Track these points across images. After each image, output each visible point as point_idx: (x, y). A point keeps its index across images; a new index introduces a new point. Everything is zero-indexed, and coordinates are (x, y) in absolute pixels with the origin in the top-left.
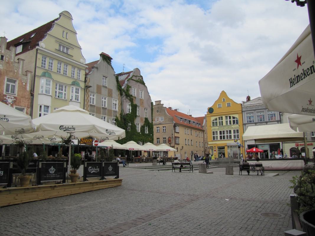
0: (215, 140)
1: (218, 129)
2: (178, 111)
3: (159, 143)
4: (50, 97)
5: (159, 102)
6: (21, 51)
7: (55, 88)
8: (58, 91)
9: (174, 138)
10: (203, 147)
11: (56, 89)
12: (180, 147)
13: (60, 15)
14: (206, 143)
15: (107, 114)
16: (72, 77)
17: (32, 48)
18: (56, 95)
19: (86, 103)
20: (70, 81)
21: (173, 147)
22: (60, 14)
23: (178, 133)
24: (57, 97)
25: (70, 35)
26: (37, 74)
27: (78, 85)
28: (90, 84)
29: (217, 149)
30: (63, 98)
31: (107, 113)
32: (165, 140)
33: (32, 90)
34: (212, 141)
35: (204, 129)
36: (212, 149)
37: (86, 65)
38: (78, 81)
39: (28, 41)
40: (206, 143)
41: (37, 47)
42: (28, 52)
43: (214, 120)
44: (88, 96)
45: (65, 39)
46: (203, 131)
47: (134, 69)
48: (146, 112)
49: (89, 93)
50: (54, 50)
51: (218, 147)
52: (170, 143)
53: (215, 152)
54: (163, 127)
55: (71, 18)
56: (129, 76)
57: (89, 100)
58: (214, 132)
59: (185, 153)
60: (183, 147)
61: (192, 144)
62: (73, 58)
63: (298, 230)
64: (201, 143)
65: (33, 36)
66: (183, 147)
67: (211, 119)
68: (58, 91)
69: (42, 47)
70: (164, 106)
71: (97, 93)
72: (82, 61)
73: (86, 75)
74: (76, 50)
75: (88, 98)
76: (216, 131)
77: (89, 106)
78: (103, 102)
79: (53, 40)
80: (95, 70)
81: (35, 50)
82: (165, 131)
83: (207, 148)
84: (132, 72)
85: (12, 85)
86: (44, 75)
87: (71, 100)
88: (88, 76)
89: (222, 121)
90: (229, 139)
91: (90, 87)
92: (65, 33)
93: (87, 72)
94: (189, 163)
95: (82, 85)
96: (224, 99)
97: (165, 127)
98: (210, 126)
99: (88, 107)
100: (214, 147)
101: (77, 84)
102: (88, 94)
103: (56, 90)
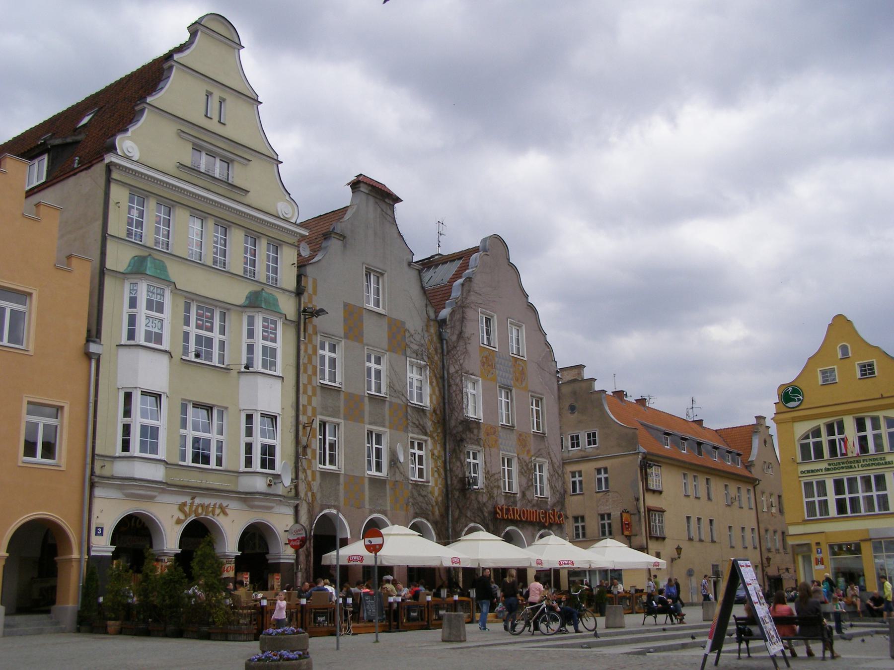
0: (818, 517)
1: (828, 470)
2: (651, 406)
3: (584, 535)
4: (165, 359)
5: (575, 371)
6: (44, 180)
7: (182, 322)
8: (193, 331)
10: (755, 548)
11: (187, 322)
12: (668, 548)
13: (194, 30)
14: (767, 531)
15: (387, 423)
16: (249, 276)
17: (87, 164)
18: (186, 350)
19: (303, 379)
20: (238, 294)
21: (643, 549)
22: (194, 27)
23: (656, 495)
24: (191, 357)
25: (234, 108)
26: (109, 265)
27: (272, 308)
28: (318, 304)
29: (826, 554)
30: (215, 361)
31: (387, 417)
33: (94, 332)
34: (805, 522)
35: (756, 473)
36: (804, 557)
37: (303, 225)
38: (268, 290)
39: (69, 140)
40: (767, 531)
41: (109, 158)
42: (71, 181)
43: (807, 437)
44: (310, 351)
45: (214, 126)
46: (753, 482)
47: (484, 241)
48: (537, 411)
49: (314, 337)
50: (170, 167)
51: (831, 547)
52: (627, 533)
53: (821, 567)
54: (599, 471)
55: (237, 41)
56: (465, 267)
57: (315, 368)
58: (808, 485)
59: (690, 573)
60: (679, 549)
61: (715, 539)
62: (250, 199)
64: (748, 534)
65: (86, 120)
66: (679, 549)
67: (793, 428)
68: (193, 331)
69: (128, 158)
70: (598, 387)
71: (346, 337)
72: (283, 208)
73: (302, 265)
74: (257, 167)
75: (314, 357)
76: (820, 478)
77: (318, 390)
78: (369, 375)
79: (169, 129)
80: (334, 244)
81: (99, 170)
82: (607, 487)
83: (773, 550)
84: (476, 250)
85: (12, 310)
86: (138, 269)
87: (247, 367)
88: (309, 270)
89: (606, 476)
90: (877, 511)
91: (320, 312)
92: (214, 103)
93: (306, 253)
95: (288, 306)
96: (844, 349)
97: (580, 473)
98: (794, 460)
99: (314, 394)
100: (814, 548)
101: (267, 302)
102: (310, 341)
103: (186, 328)
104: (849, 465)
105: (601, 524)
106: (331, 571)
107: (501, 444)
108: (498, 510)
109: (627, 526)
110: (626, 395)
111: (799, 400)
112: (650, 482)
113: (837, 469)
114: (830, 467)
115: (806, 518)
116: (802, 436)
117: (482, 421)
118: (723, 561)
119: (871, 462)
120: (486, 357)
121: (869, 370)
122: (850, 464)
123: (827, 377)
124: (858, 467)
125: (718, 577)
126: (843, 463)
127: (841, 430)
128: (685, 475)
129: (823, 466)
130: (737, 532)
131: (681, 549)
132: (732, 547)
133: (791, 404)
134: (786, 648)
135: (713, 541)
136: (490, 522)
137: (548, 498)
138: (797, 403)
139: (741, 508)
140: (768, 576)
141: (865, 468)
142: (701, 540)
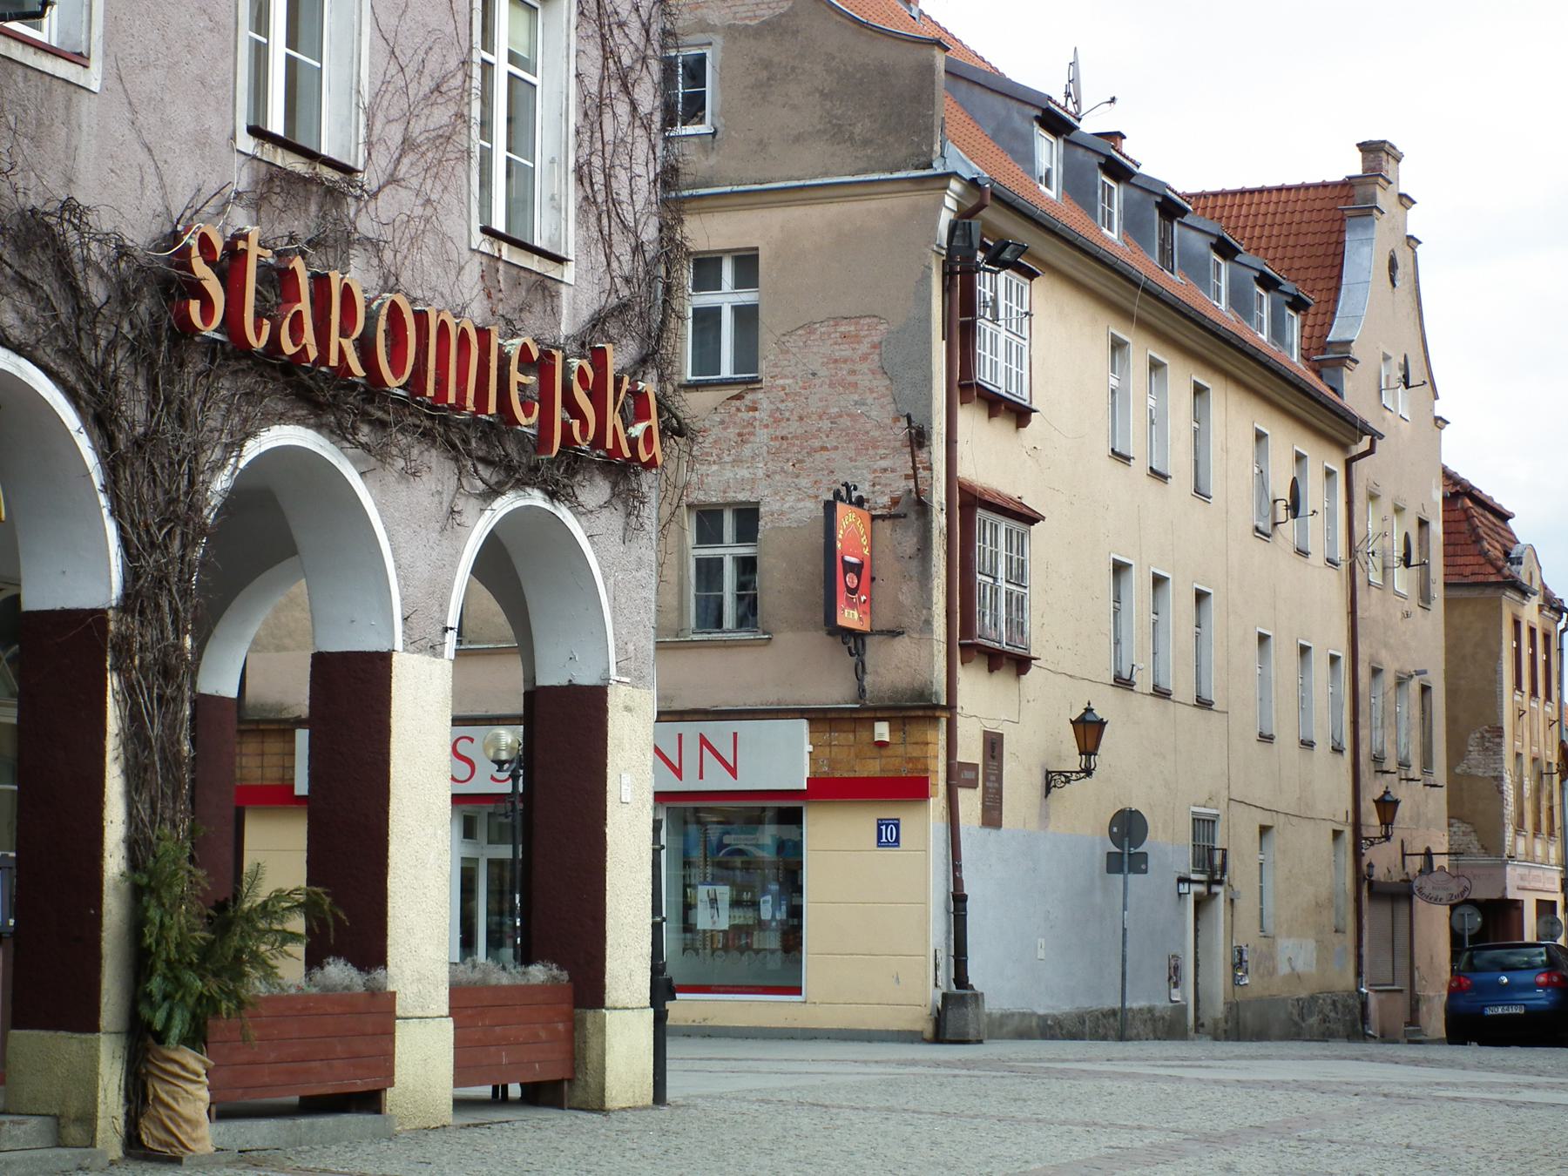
9: (939, 520)
10: (1338, 750)
14: (1376, 672)
32: (729, 552)
35: (1356, 394)
60: (1089, 730)
66: (1089, 730)
89: (747, 297)
97: (747, 266)
105: (699, 561)
106: (565, 976)
108: (201, 269)
109: (851, 580)
112: (983, 351)
125: (1211, 882)
128: (1117, 345)
131: (1101, 724)
132: (1267, 738)
135: (1203, 704)
136: (121, 361)
137: (560, 260)
139: (1302, 553)
140: (1371, 884)
142: (1161, 693)
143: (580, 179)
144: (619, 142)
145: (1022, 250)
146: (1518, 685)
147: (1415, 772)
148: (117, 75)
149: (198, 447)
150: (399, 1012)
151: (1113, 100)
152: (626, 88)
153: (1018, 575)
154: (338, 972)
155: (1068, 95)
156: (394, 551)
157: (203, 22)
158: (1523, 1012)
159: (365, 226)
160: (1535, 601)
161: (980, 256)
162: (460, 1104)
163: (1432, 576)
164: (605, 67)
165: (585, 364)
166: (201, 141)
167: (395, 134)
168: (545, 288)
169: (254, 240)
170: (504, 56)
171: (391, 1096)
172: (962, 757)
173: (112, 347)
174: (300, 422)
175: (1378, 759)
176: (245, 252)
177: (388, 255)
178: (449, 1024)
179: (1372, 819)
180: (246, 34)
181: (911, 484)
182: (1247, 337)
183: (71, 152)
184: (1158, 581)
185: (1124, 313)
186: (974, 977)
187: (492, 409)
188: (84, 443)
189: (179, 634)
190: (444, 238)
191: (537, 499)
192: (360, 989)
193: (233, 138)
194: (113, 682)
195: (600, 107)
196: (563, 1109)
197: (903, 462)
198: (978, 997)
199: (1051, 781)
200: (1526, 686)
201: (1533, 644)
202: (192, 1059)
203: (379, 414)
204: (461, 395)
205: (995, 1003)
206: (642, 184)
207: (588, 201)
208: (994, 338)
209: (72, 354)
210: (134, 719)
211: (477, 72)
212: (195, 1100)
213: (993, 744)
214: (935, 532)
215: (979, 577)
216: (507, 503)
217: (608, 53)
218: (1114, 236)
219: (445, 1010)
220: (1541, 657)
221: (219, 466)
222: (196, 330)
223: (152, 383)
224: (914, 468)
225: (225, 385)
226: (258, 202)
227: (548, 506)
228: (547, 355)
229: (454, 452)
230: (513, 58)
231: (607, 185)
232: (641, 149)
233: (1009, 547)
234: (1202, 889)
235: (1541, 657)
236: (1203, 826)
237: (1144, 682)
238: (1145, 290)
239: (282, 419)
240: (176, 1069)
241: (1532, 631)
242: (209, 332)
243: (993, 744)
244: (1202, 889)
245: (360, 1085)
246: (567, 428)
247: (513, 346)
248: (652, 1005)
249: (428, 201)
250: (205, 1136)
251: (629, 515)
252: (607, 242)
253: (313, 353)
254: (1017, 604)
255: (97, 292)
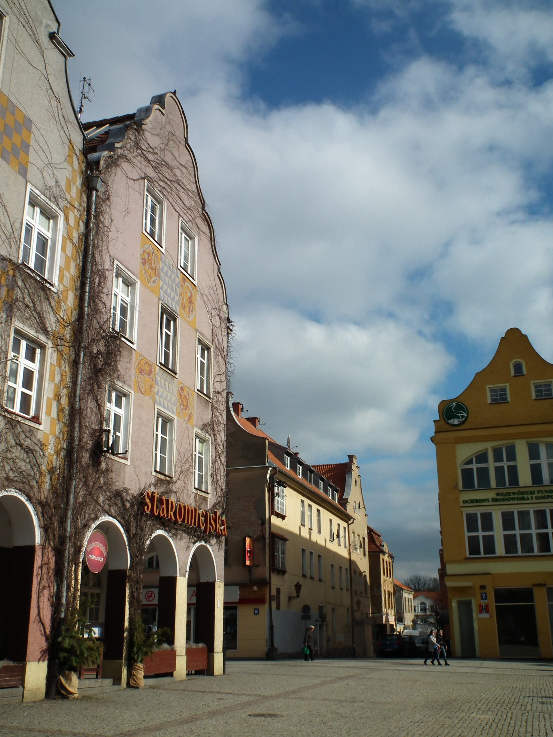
9: (267, 541)
10: (347, 590)
53: (485, 615)
60: (298, 587)
63: (186, 646)
66: (298, 587)
89: (511, 463)
94: (70, 589)
96: (518, 368)
104: (521, 496)
106: (206, 646)
107: (157, 393)
108: (148, 500)
110: (242, 409)
111: (463, 417)
113: (507, 500)
114: (498, 497)
115: (468, 555)
116: (464, 461)
117: (134, 347)
118: (326, 602)
119: (547, 494)
120: (149, 254)
121: (546, 390)
122: (522, 496)
123: (501, 395)
124: (532, 499)
126: (514, 493)
127: (512, 456)
128: (302, 501)
129: (490, 495)
130: (336, 569)
133: (453, 421)
134: (152, 644)
135: (320, 580)
138: (460, 420)
141: (539, 501)
142: (312, 578)
143: (211, 477)
144: (218, 469)
145: (284, 482)
146: (384, 574)
147: (364, 595)
148: (132, 462)
149: (144, 536)
150: (177, 655)
151: (297, 446)
152: (220, 458)
153: (283, 553)
154: (166, 646)
155: (287, 445)
156: (178, 555)
157: (147, 450)
158: (417, 645)
159: (174, 489)
160: (387, 555)
161: (275, 484)
162: (188, 674)
163: (366, 550)
164: (216, 454)
165: (213, 515)
166: (146, 474)
167: (179, 470)
168: (205, 499)
169: (156, 494)
170: (198, 452)
171: (174, 672)
172: (272, 594)
173: (130, 516)
174: (162, 529)
175: (356, 592)
176: (155, 496)
177: (178, 494)
178: (185, 657)
179: (355, 606)
180: (154, 452)
181: (261, 533)
182: (327, 498)
183: (124, 477)
184: (311, 553)
185: (303, 495)
186: (275, 645)
187: (197, 525)
188: (124, 535)
189: (140, 574)
190: (188, 490)
191: (203, 543)
192: (170, 649)
193: (152, 473)
194: (127, 585)
195: (215, 462)
196: (205, 675)
197: (260, 528)
198: (276, 649)
199: (290, 599)
200: (386, 574)
201: (384, 563)
202: (141, 665)
203: (176, 527)
204: (191, 523)
205: (280, 650)
206: (223, 477)
207: (213, 481)
208: (278, 501)
209: (123, 518)
210: (131, 592)
211: (194, 456)
212: (140, 674)
213: (278, 591)
214: (267, 543)
215: (276, 553)
216: (198, 544)
217: (217, 451)
218: (288, 469)
219: (185, 654)
220: (388, 568)
221: (147, 539)
222: (145, 512)
223: (137, 523)
224: (262, 529)
225: (149, 523)
226: (155, 485)
227: (205, 544)
228: (206, 513)
229: (189, 534)
230: (199, 453)
231: (216, 478)
232: (222, 469)
233: (281, 547)
234: (321, 623)
235: (388, 568)
236: (321, 608)
237: (308, 576)
238: (308, 490)
239: (158, 529)
240: (137, 667)
241: (387, 562)
242: (148, 512)
243: (278, 591)
244: (321, 623)
245: (169, 671)
246: (210, 528)
247: (200, 512)
248: (223, 652)
249: (185, 483)
250: (142, 682)
251: (219, 546)
252: (216, 489)
253: (166, 516)
254: (283, 559)
255: (128, 505)
